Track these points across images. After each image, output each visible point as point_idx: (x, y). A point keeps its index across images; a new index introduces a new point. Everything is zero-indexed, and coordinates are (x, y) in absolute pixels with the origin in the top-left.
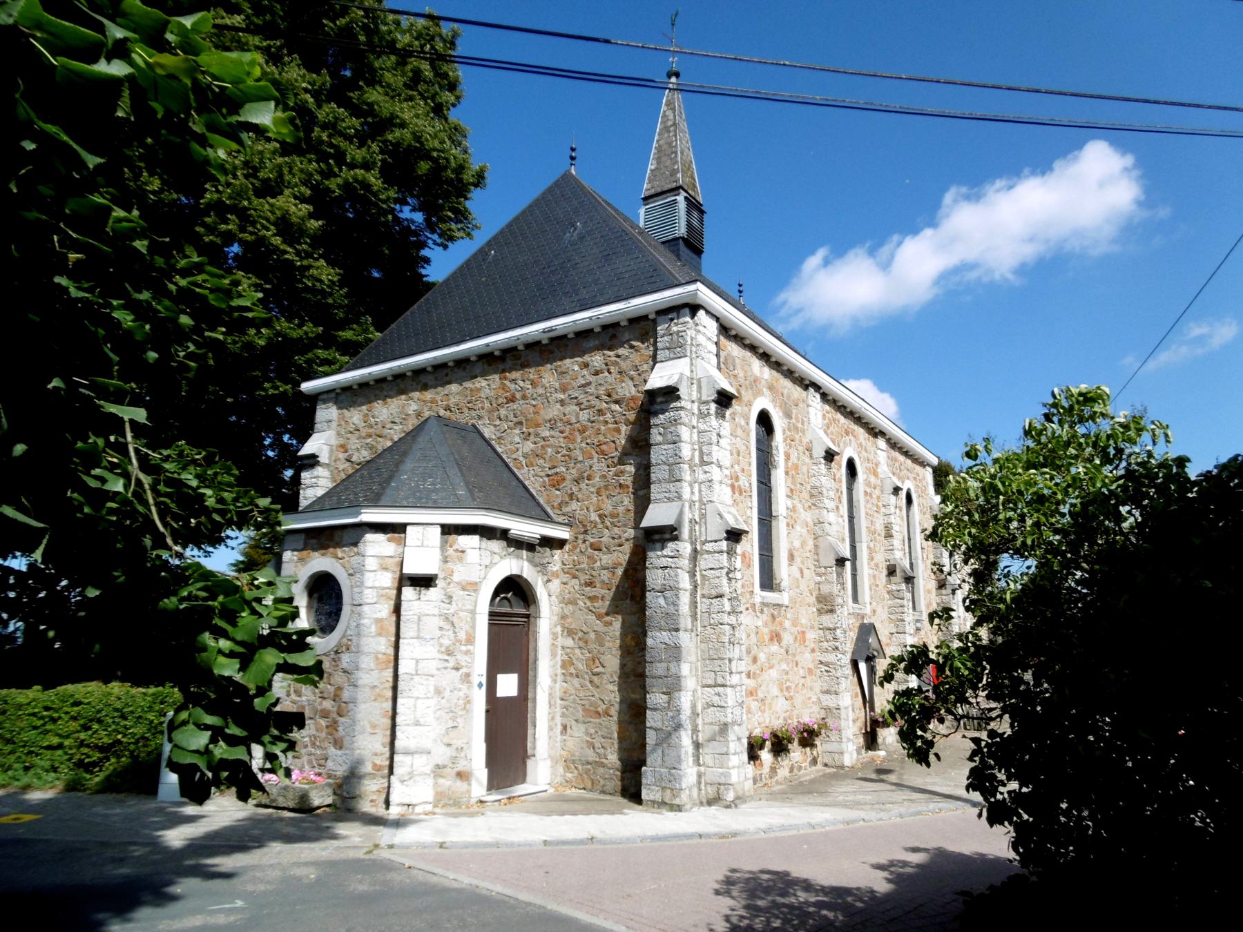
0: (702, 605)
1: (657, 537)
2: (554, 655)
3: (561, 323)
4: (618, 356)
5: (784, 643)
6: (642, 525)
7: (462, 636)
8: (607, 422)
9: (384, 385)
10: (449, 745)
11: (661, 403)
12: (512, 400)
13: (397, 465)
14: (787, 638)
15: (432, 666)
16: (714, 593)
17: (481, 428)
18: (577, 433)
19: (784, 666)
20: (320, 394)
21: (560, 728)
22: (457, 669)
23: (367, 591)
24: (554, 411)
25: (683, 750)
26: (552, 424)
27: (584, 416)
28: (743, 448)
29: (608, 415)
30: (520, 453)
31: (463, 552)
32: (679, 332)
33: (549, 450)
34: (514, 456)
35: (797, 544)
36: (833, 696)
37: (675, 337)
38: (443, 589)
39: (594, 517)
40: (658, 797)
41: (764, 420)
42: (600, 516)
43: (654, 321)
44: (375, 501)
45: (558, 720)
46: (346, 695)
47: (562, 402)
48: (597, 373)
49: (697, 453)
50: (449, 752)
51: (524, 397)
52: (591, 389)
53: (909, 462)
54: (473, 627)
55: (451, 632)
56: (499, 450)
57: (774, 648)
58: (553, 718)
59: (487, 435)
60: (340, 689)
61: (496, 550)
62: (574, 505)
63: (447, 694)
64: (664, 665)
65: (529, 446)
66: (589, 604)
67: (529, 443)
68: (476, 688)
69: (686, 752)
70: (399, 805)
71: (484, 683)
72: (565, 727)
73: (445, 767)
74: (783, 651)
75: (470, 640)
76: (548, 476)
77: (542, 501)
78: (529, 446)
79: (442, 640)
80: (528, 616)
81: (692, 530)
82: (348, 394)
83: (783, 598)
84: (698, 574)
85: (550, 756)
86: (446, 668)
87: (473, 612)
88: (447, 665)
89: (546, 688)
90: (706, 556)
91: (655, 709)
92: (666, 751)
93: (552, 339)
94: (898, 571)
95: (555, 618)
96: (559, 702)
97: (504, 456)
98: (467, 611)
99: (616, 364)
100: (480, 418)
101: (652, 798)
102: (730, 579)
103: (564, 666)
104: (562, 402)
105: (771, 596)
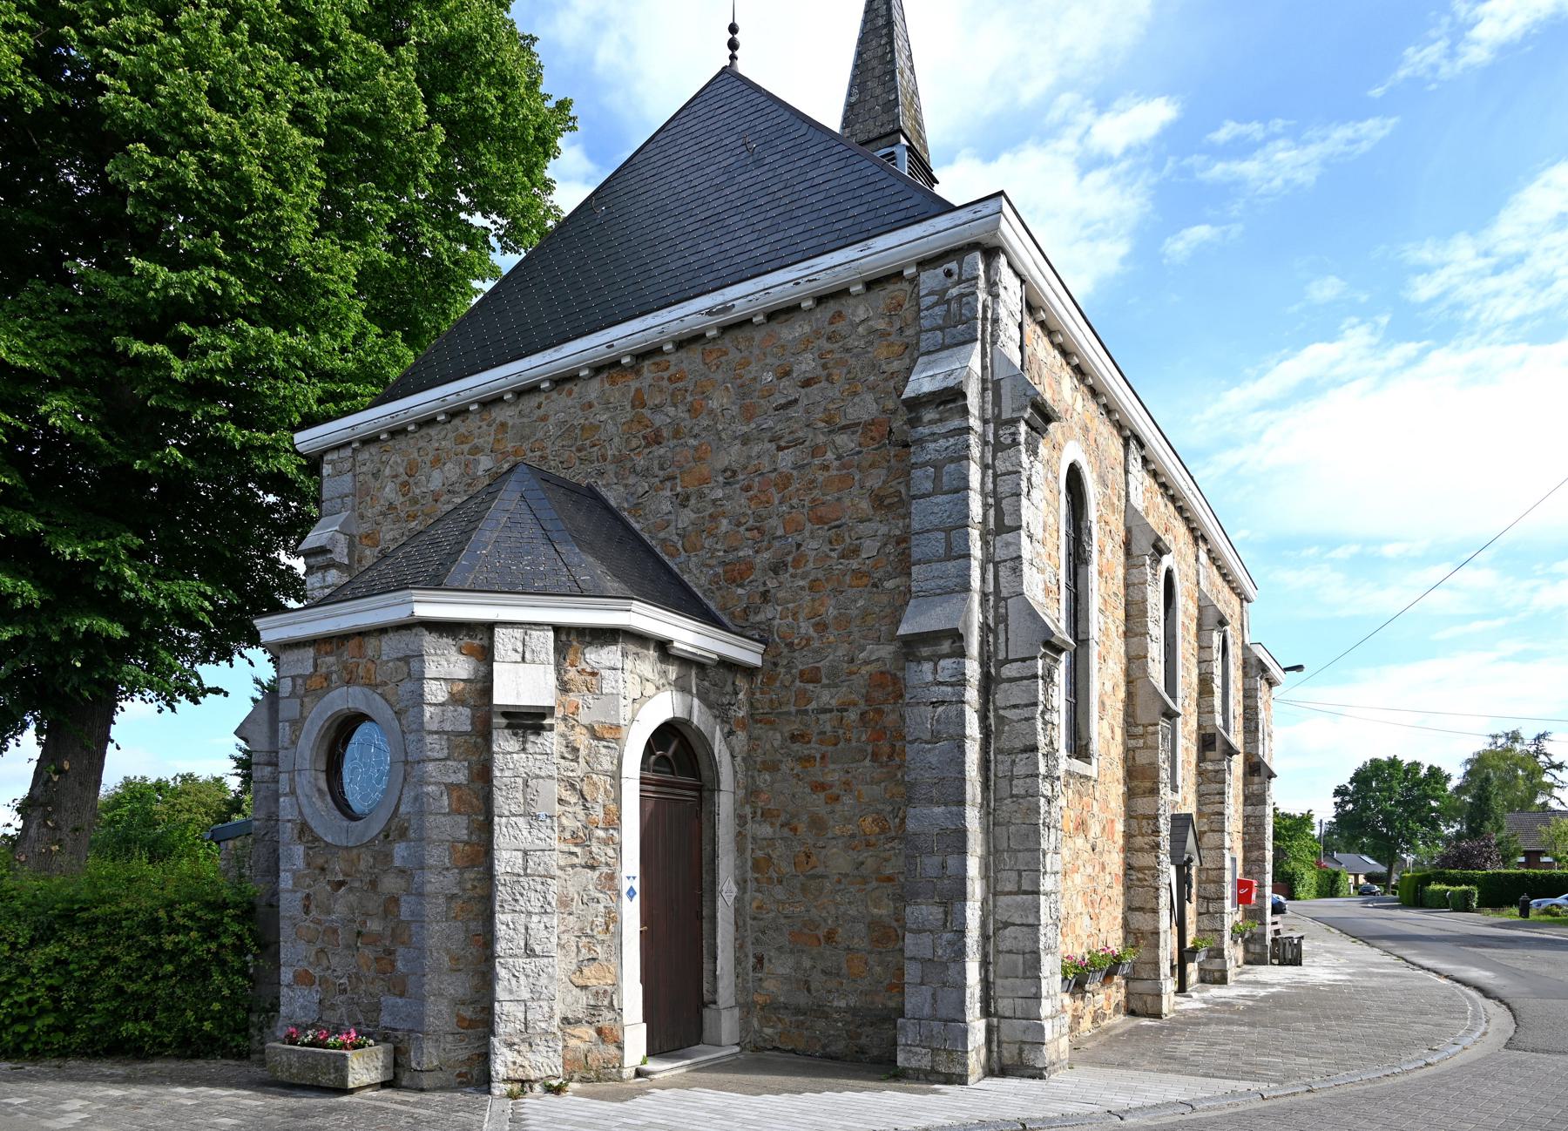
0: (1001, 767)
1: (925, 651)
2: (740, 850)
3: (742, 296)
4: (848, 350)
5: (1091, 835)
6: (901, 631)
7: (598, 813)
8: (826, 468)
9: (433, 432)
10: (584, 988)
11: (931, 422)
12: (657, 440)
13: (466, 534)
14: (1095, 829)
15: (555, 860)
16: (1019, 745)
17: (603, 492)
18: (773, 490)
19: (1089, 870)
20: (326, 452)
21: (752, 960)
22: (593, 868)
23: (429, 739)
24: (732, 455)
25: (968, 992)
26: (730, 474)
27: (786, 460)
28: (1051, 520)
29: (830, 455)
30: (672, 528)
31: (594, 674)
32: (962, 295)
33: (725, 522)
34: (662, 535)
35: (1108, 687)
36: (1148, 916)
37: (954, 306)
38: (563, 735)
39: (806, 628)
40: (925, 1063)
41: (1074, 474)
42: (816, 625)
43: (913, 280)
44: (436, 583)
45: (750, 949)
46: (405, 911)
47: (745, 440)
48: (807, 383)
49: (992, 512)
50: (584, 999)
51: (677, 434)
52: (796, 413)
53: (1226, 589)
54: (618, 800)
55: (579, 809)
56: (636, 526)
57: (1080, 841)
58: (741, 946)
59: (613, 503)
60: (394, 900)
61: (650, 676)
62: (768, 612)
63: (576, 906)
64: (937, 860)
65: (686, 517)
66: (798, 769)
67: (687, 511)
68: (625, 898)
69: (973, 995)
70: (508, 1080)
71: (637, 889)
72: (760, 960)
73: (578, 1021)
74: (1089, 846)
75: (613, 822)
76: (724, 563)
77: (712, 606)
78: (686, 517)
79: (564, 821)
80: (699, 789)
81: (984, 642)
82: (374, 449)
83: (1092, 771)
84: (991, 715)
85: (738, 1004)
86: (573, 866)
87: (616, 777)
88: (576, 861)
89: (730, 901)
90: (1005, 686)
91: (919, 931)
92: (940, 994)
93: (725, 329)
94: (1218, 743)
95: (741, 793)
96: (749, 922)
97: (646, 536)
98: (605, 773)
99: (842, 363)
100: (601, 474)
101: (914, 1064)
102: (1045, 723)
103: (756, 866)
104: (745, 440)
105: (1078, 766)
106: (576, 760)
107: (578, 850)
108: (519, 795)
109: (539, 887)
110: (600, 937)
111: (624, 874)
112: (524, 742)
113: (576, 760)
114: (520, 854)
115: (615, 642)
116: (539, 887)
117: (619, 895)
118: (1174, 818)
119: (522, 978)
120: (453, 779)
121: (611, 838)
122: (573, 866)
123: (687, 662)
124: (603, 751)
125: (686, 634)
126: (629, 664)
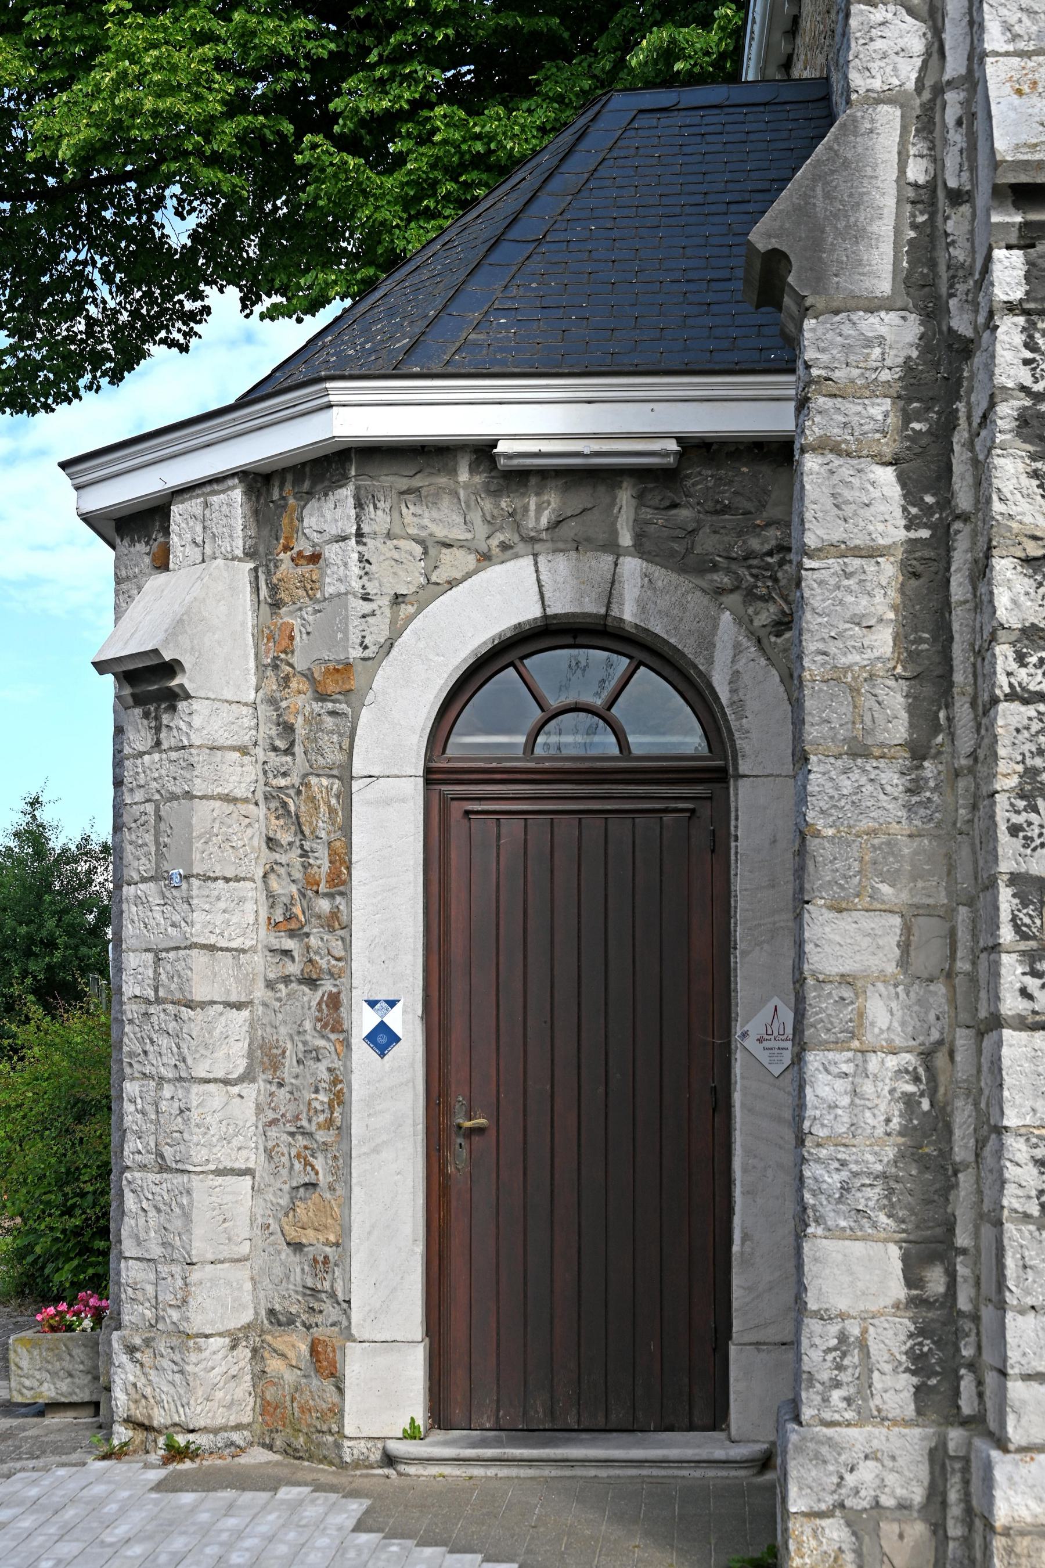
63: (289, 1068)
86: (286, 980)
106: (289, 751)
107: (289, 944)
108: (149, 838)
109: (172, 1026)
110: (321, 1136)
111: (358, 997)
112: (158, 729)
113: (289, 751)
114: (150, 956)
115: (341, 481)
116: (172, 1026)
117: (347, 1044)
118: (908, 528)
119: (152, 1213)
120: (818, 840)
121: (335, 914)
122: (286, 980)
123: (583, 477)
124: (329, 722)
125: (528, 417)
126: (378, 520)
